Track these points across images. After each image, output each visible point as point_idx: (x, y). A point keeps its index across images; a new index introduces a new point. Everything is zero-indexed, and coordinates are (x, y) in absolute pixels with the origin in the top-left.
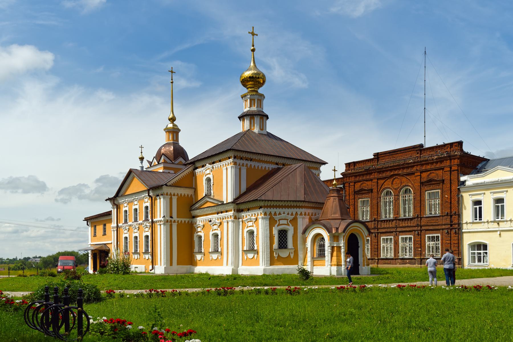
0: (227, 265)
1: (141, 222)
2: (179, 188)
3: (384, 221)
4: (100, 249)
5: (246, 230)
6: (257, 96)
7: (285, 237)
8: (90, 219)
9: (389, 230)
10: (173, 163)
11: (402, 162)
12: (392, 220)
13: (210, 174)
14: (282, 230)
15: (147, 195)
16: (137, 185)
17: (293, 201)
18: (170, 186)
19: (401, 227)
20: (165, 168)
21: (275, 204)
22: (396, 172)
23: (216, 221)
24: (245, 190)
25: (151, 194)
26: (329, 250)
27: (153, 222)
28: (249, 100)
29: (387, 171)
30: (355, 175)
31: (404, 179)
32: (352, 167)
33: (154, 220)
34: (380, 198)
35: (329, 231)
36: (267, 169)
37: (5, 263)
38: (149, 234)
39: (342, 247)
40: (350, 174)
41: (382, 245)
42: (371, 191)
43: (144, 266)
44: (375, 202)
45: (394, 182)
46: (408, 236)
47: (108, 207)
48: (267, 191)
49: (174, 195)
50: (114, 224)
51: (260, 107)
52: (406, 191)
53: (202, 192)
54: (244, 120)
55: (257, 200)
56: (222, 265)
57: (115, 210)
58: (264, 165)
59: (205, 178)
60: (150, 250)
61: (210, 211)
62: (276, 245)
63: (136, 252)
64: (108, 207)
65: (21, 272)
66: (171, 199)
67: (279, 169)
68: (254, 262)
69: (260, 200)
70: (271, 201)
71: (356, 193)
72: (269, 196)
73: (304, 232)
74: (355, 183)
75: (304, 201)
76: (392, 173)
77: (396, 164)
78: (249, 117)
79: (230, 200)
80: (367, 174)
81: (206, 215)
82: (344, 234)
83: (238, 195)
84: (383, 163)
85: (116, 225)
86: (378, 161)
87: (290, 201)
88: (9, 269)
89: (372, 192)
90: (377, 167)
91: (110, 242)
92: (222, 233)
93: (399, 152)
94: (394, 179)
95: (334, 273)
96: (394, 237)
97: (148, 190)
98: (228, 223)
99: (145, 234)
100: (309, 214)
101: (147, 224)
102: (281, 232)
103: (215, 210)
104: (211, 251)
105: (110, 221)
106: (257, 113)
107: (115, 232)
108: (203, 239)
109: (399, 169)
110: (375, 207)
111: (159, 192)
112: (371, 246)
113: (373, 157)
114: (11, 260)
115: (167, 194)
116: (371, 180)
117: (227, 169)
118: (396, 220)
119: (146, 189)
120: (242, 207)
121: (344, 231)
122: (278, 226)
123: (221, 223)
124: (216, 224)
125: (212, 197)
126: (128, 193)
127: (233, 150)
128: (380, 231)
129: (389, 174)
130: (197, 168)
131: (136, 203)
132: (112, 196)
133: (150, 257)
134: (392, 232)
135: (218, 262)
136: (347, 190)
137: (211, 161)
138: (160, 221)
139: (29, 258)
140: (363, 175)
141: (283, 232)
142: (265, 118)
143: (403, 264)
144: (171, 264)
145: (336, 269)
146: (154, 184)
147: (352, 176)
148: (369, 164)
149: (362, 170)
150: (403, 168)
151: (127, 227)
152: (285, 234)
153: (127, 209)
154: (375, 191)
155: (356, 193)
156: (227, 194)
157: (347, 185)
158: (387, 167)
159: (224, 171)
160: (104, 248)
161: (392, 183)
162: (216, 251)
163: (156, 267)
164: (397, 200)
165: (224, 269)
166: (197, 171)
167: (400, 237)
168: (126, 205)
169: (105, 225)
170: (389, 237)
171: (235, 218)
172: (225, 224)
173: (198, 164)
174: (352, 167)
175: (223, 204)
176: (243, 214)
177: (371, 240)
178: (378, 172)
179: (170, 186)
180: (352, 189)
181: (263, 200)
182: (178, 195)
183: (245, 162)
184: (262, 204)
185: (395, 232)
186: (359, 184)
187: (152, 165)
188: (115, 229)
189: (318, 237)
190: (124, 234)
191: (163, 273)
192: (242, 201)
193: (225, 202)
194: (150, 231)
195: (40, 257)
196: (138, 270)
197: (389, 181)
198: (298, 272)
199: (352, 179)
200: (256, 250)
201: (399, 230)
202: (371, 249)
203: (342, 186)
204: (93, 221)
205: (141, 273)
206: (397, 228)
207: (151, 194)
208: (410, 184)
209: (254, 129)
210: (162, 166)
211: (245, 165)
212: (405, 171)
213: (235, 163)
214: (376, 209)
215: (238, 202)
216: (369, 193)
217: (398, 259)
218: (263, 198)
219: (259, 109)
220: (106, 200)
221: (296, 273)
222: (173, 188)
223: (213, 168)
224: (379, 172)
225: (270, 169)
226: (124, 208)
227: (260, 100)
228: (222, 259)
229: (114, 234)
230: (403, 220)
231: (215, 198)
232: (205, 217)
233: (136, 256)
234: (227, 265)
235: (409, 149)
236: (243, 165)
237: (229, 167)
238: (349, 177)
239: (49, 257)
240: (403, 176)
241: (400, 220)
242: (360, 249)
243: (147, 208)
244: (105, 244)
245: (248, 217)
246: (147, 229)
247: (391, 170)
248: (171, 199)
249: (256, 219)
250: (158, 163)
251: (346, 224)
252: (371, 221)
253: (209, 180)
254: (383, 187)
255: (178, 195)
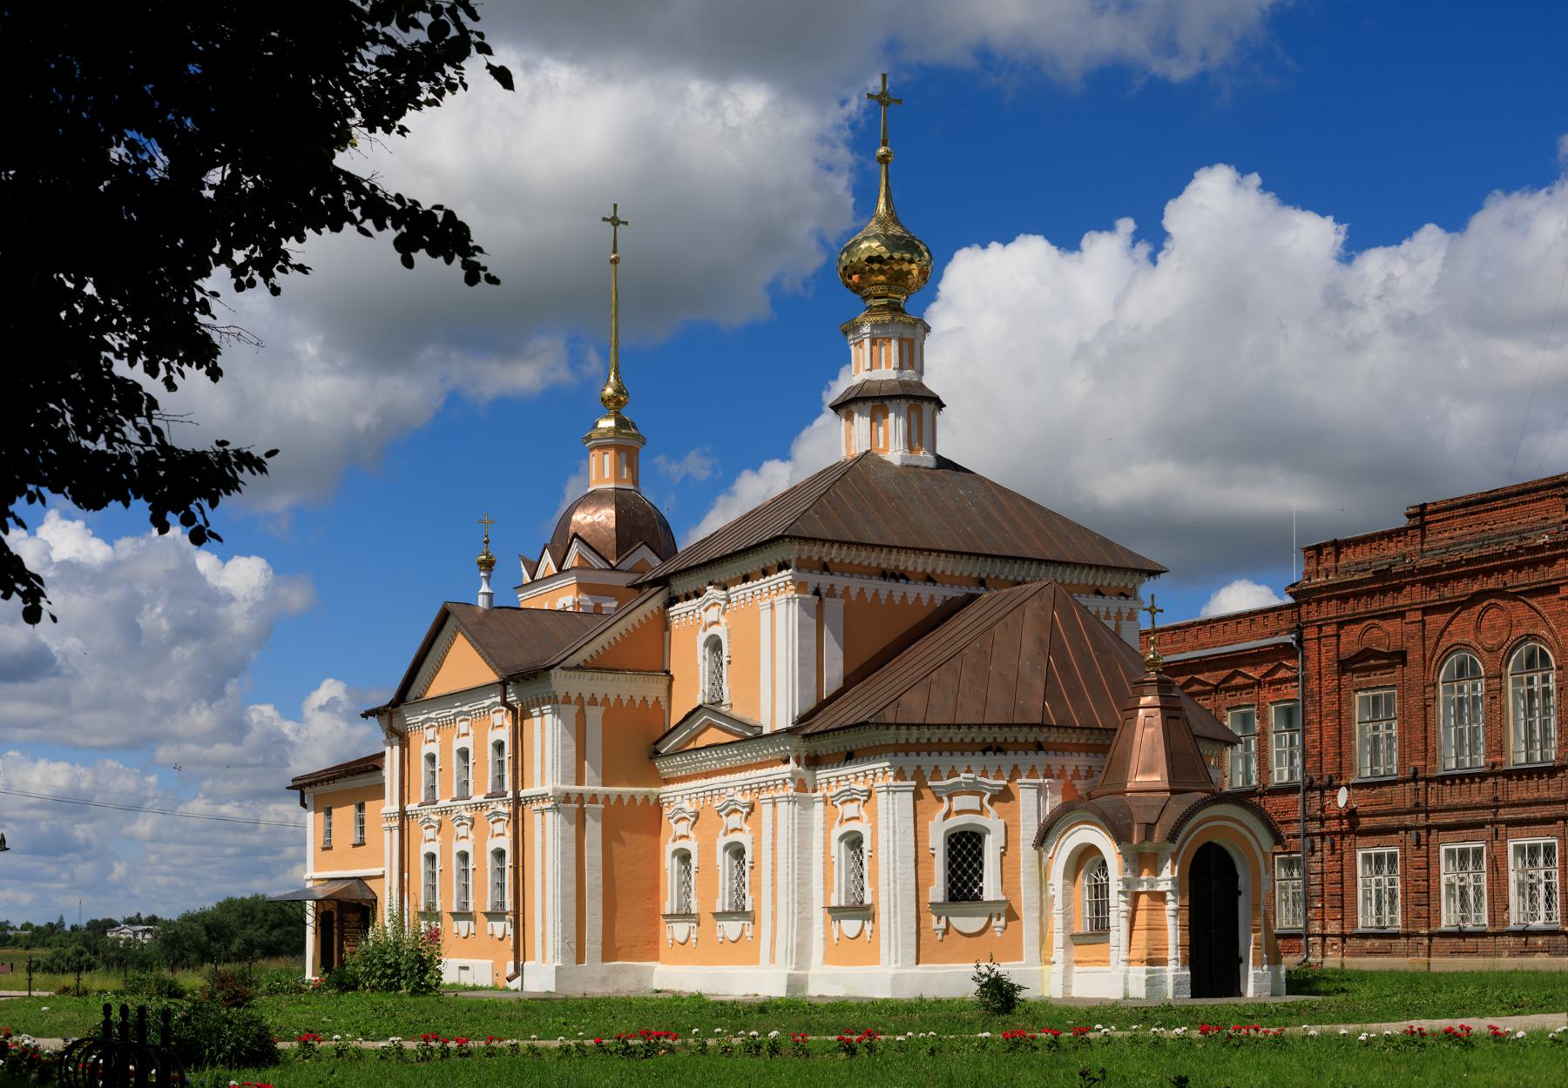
0: (772, 959)
1: (479, 798)
2: (610, 677)
3: (1452, 778)
4: (347, 897)
5: (838, 831)
6: (900, 329)
7: (975, 859)
8: (310, 785)
9: (1468, 816)
10: (613, 568)
11: (1511, 544)
12: (1483, 777)
13: (717, 623)
14: (963, 834)
15: (498, 699)
16: (463, 666)
17: (1001, 726)
18: (578, 668)
19: (1514, 805)
20: (582, 587)
21: (936, 736)
22: (1491, 583)
23: (739, 797)
24: (840, 684)
25: (511, 698)
26: (1124, 907)
27: (517, 801)
28: (867, 342)
29: (1458, 578)
30: (1341, 593)
31: (1519, 610)
32: (1330, 564)
33: (523, 793)
34: (1435, 685)
35: (1120, 837)
36: (925, 602)
37: (16, 942)
38: (506, 843)
39: (1170, 896)
40: (1320, 590)
41: (1443, 879)
42: (1400, 657)
43: (489, 962)
44: (1415, 701)
45: (1485, 623)
46: (1542, 841)
47: (367, 738)
48: (912, 688)
49: (831, 592)
50: (390, 805)
51: (912, 366)
52: (1530, 664)
53: (690, 691)
54: (849, 417)
55: (866, 723)
56: (755, 961)
57: (397, 748)
58: (913, 590)
59: (702, 637)
60: (509, 906)
61: (711, 761)
62: (937, 891)
63: (463, 915)
64: (367, 738)
65: (69, 980)
66: (581, 718)
67: (971, 598)
68: (862, 951)
69: (878, 725)
70: (918, 726)
71: (1345, 666)
72: (914, 706)
73: (1043, 838)
74: (1341, 625)
75: (1041, 726)
76: (1476, 588)
77: (1490, 551)
78: (870, 405)
79: (784, 721)
80: (1384, 591)
81: (707, 775)
82: (1174, 847)
83: (812, 704)
84: (1446, 541)
85: (396, 808)
86: (1424, 536)
87: (990, 726)
88: (30, 970)
89: (1404, 663)
90: (1423, 562)
91: (376, 871)
92: (757, 841)
93: (1500, 503)
94: (1486, 610)
95: (1138, 991)
96: (1490, 843)
97: (504, 684)
98: (774, 804)
99: (493, 844)
100: (1063, 770)
101: (500, 808)
102: (959, 840)
103: (733, 757)
104: (719, 910)
105: (378, 792)
106: (900, 392)
107: (396, 833)
108: (694, 861)
109: (1502, 570)
110: (1417, 723)
111: (534, 689)
112: (1405, 883)
113: (1403, 522)
114: (38, 929)
115: (567, 700)
116: (1402, 615)
117: (772, 606)
118: (1495, 775)
119: (492, 677)
120: (824, 746)
121: (1172, 837)
122: (947, 816)
123: (752, 807)
124: (735, 811)
125: (724, 709)
126: (430, 695)
127: (793, 538)
128: (1435, 819)
129: (1463, 588)
130: (673, 601)
131: (463, 727)
132: (385, 696)
133: (510, 931)
134: (1480, 825)
135: (744, 951)
136: (1313, 656)
137: (721, 573)
138: (543, 797)
139: (111, 924)
140: (1371, 594)
141: (969, 840)
142: (927, 408)
143: (1522, 953)
144: (580, 959)
145: (1144, 976)
146: (521, 659)
147: (1329, 599)
148: (1392, 549)
149: (1364, 576)
150: (1518, 567)
151: (435, 818)
152: (975, 846)
153: (434, 748)
154: (1414, 657)
155: (1345, 666)
156: (776, 702)
157: (1310, 633)
158: (1458, 564)
159: (765, 615)
160: (357, 894)
161: (1478, 628)
162: (738, 912)
163: (528, 965)
164: (1496, 694)
165: (757, 980)
166: (676, 609)
167: (1511, 845)
168: (430, 734)
169: (361, 807)
170: (1470, 846)
171: (801, 786)
172: (767, 810)
173: (679, 587)
174: (1329, 563)
175: (759, 737)
176: (822, 774)
177: (1404, 859)
178: (1425, 582)
179: (578, 668)
180: (1329, 654)
181: (888, 725)
182: (606, 699)
183: (840, 582)
184: (889, 736)
185: (1492, 823)
186: (1357, 628)
187: (539, 576)
188: (396, 823)
189: (1086, 857)
190: (425, 842)
191: (553, 989)
192: (822, 728)
193: (766, 731)
194: (509, 833)
195: (153, 920)
196: (467, 979)
197: (1467, 617)
198: (975, 987)
199: (1331, 609)
200: (868, 908)
201: (1505, 814)
202: (1405, 893)
203: (1289, 639)
204: (319, 789)
205: (475, 988)
206: (1498, 807)
207: (511, 698)
208: (1544, 632)
209: (886, 449)
210: (572, 580)
211: (839, 590)
212: (1525, 578)
213: (801, 587)
214: (1419, 735)
215: (809, 731)
216: (1393, 666)
217: (1502, 934)
218: (890, 717)
219: (909, 374)
220: (366, 715)
221: (971, 990)
222: (588, 675)
223: (729, 601)
224: (1430, 584)
225: (938, 603)
226: (426, 741)
227: (911, 342)
228: (756, 937)
229: (391, 841)
230: (1452, 779)
231: (737, 713)
232: (704, 782)
233: (463, 926)
234: (772, 959)
235: (1536, 490)
236: (831, 592)
237: (780, 600)
238: (1319, 602)
239: (189, 918)
240: (1514, 597)
241: (1508, 774)
242: (1241, 899)
243: (499, 746)
244: (360, 879)
245: (844, 786)
246: (498, 827)
247: (1472, 575)
248: (581, 718)
249: (870, 794)
250: (559, 569)
251: (1184, 808)
252: (1404, 781)
253: (715, 645)
254: (1445, 643)
255: (606, 699)
